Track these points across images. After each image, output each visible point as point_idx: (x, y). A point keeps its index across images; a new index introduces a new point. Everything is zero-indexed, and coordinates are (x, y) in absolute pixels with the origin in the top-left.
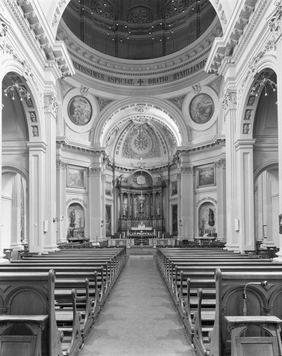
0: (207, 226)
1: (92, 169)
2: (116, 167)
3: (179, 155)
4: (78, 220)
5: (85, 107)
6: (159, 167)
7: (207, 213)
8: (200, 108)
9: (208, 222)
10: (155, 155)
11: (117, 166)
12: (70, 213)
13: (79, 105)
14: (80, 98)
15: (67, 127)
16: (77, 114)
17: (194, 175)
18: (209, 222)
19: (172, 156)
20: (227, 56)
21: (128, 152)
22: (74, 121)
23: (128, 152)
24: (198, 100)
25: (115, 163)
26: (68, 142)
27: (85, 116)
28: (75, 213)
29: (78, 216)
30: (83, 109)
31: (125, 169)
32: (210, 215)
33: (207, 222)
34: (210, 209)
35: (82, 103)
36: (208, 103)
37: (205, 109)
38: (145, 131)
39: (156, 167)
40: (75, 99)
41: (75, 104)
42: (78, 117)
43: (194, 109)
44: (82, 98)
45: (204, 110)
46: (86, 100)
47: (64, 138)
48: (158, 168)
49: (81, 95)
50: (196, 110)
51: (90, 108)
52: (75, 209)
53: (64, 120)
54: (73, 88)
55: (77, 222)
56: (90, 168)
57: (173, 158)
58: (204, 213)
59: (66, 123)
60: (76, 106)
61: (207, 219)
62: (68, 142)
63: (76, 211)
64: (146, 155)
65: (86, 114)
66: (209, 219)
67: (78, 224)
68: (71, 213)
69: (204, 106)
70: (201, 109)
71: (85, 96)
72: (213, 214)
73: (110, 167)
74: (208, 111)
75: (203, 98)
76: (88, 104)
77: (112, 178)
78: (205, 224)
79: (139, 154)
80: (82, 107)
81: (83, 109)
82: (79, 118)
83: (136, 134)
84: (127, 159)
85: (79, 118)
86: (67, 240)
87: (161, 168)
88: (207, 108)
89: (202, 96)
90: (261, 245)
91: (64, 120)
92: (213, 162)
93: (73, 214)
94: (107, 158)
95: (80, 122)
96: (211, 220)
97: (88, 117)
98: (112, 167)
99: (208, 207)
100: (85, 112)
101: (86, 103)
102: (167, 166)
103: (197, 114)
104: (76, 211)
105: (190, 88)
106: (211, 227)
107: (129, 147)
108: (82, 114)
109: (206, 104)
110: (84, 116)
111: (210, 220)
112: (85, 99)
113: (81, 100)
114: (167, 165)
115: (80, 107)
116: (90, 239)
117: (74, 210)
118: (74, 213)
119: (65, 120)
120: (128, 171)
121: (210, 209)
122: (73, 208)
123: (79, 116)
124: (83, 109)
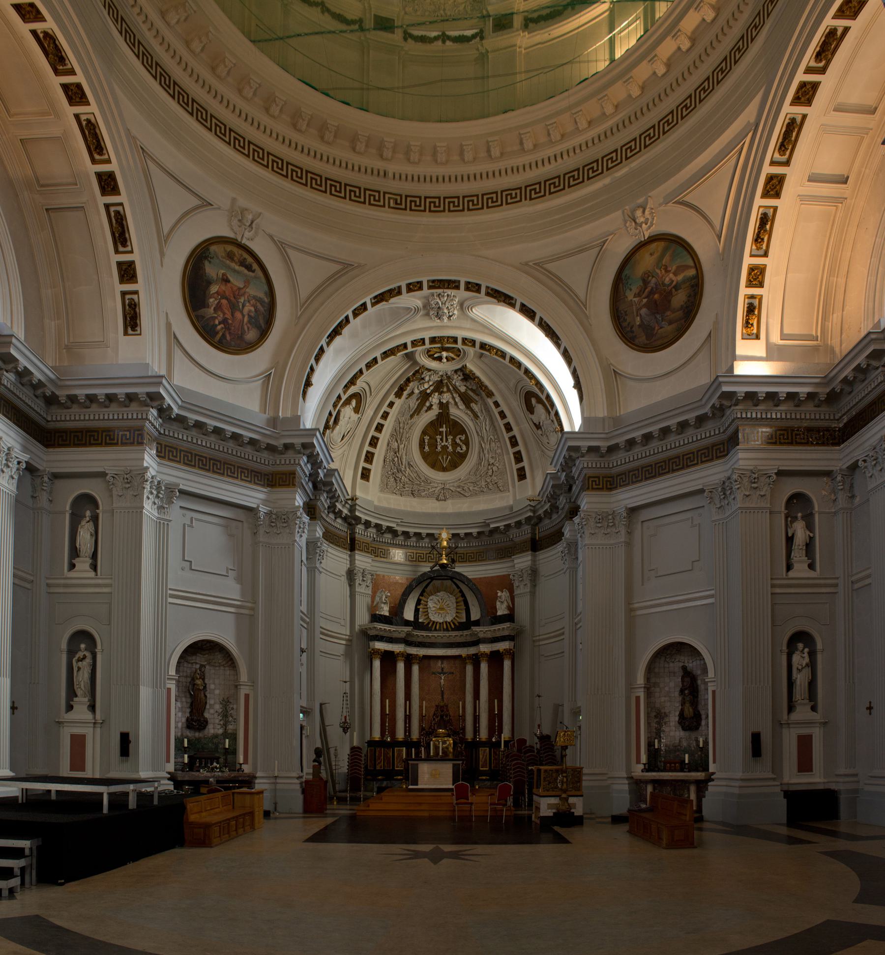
0: (672, 734)
1: (269, 514)
2: (358, 520)
3: (574, 470)
4: (218, 707)
5: (247, 282)
6: (501, 525)
7: (672, 684)
8: (652, 292)
9: (677, 719)
10: (487, 485)
11: (364, 517)
12: (189, 680)
13: (223, 275)
14: (229, 248)
15: (178, 354)
16: (218, 308)
17: (629, 544)
18: (681, 715)
19: (549, 477)
20: (565, 493)
21: (399, 475)
22: (207, 332)
23: (399, 475)
24: (646, 261)
25: (357, 507)
26: (180, 402)
27: (246, 319)
28: (206, 681)
29: (217, 692)
30: (238, 293)
31: (390, 530)
32: (686, 692)
33: (674, 718)
34: (684, 668)
35: (237, 268)
36: (681, 269)
37: (670, 292)
38: (458, 399)
39: (492, 526)
40: (208, 249)
41: (211, 270)
42: (220, 318)
43: (630, 296)
44: (235, 250)
45: (667, 296)
46: (250, 260)
47: (157, 380)
48: (498, 527)
49: (231, 235)
50: (636, 299)
51: (266, 288)
52: (209, 664)
53: (169, 325)
54: (207, 204)
55: (212, 713)
56: (263, 509)
57: (553, 486)
58: (662, 685)
59: (175, 337)
60: (215, 277)
61: (672, 705)
62: (180, 402)
63: (209, 671)
64: (459, 487)
65: (250, 311)
66: (683, 704)
67: (217, 721)
68: (193, 679)
69: (667, 281)
70: (656, 296)
71: (244, 241)
72: (697, 686)
73: (339, 520)
74: (679, 299)
75: (665, 250)
76: (259, 273)
77: (348, 562)
78: (665, 723)
79: (438, 483)
80: (237, 282)
81: (239, 289)
82: (224, 321)
83: (429, 412)
84: (398, 497)
85: (224, 321)
86: (169, 779)
87: (508, 526)
88: (677, 287)
89: (661, 245)
90: (709, 784)
91: (169, 325)
92: (700, 487)
93: (199, 682)
94: (328, 480)
95: (228, 338)
96: (689, 711)
97: (258, 327)
98: (345, 519)
99: (675, 666)
100: (247, 304)
101: (249, 268)
102: (528, 519)
103: (638, 316)
104: (213, 671)
105: (615, 219)
106: (687, 733)
107: (404, 457)
108: (233, 307)
109: (675, 274)
110: (243, 316)
111: (686, 710)
112: (246, 256)
113: (230, 256)
114: (531, 514)
115: (226, 281)
116: (255, 778)
117: (202, 666)
118: (203, 678)
119: (172, 322)
120: (401, 538)
121: (684, 668)
122: (199, 659)
123: (224, 314)
124: (238, 293)
